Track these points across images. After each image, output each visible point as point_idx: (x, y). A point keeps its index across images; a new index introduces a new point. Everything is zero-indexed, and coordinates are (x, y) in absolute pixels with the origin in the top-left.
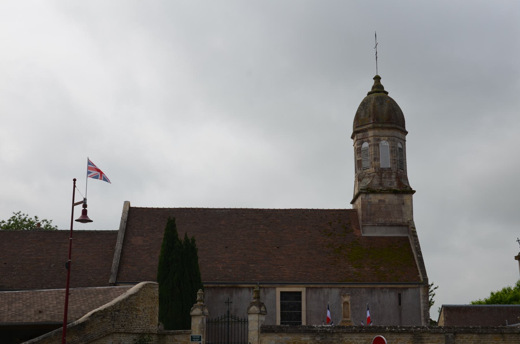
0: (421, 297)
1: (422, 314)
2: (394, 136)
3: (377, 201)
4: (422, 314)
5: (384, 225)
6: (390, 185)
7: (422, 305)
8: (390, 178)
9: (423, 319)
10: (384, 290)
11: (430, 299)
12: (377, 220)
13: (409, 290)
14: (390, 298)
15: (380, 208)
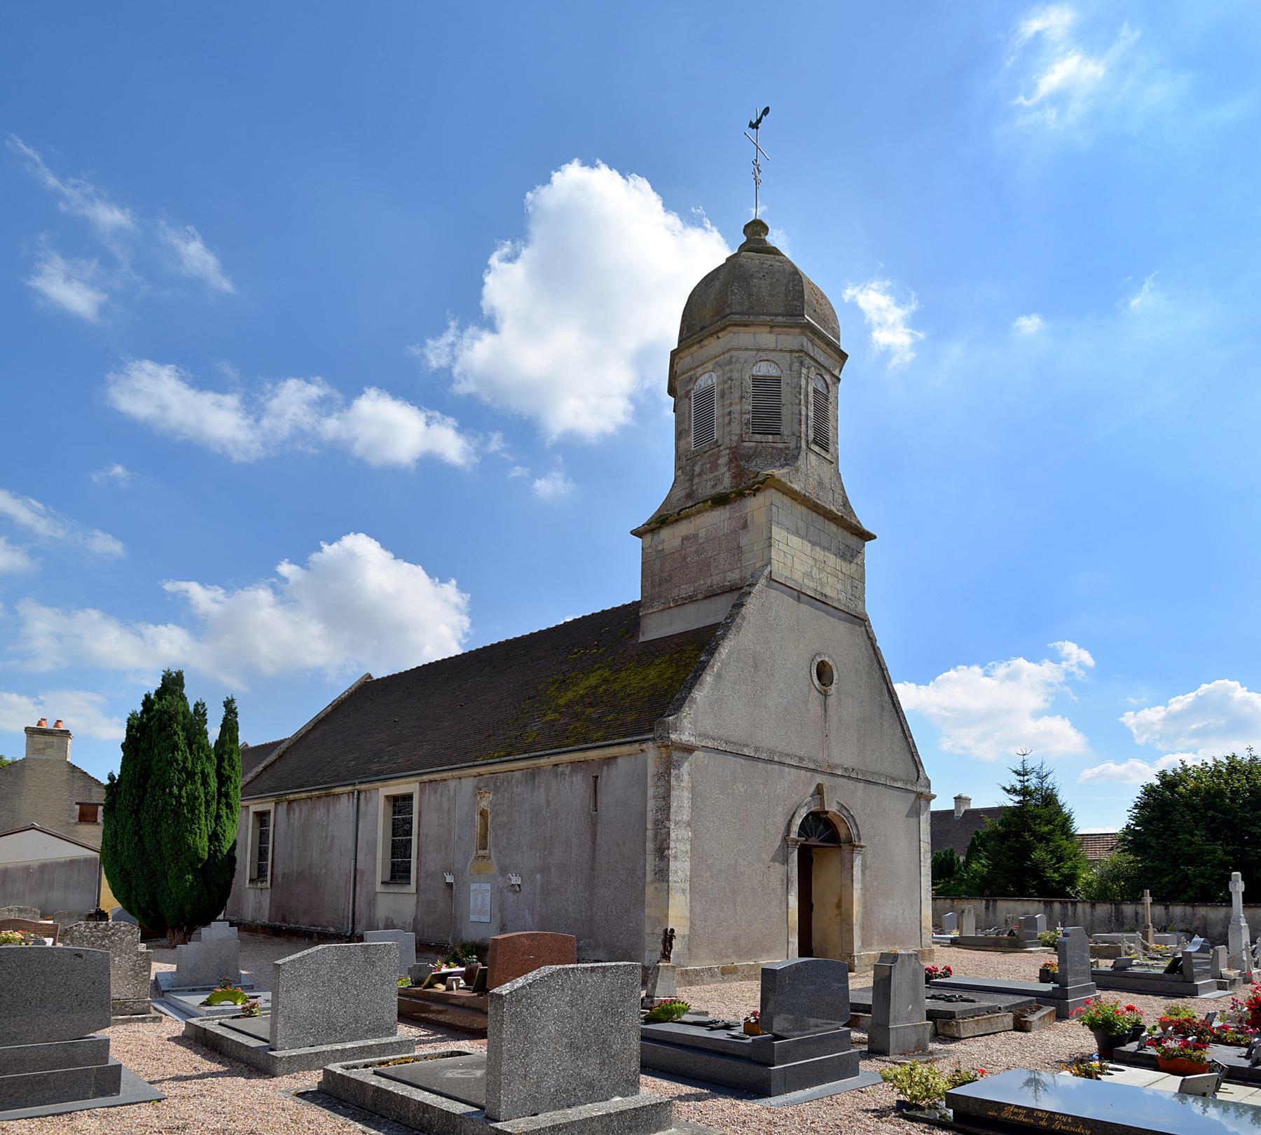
0: (650, 781)
1: (650, 834)
2: (729, 350)
3: (677, 542)
4: (650, 834)
5: (692, 599)
6: (713, 487)
7: (651, 804)
8: (715, 466)
9: (650, 846)
10: (560, 769)
11: (203, 845)
12: (676, 591)
13: (619, 760)
14: (573, 790)
15: (685, 558)
